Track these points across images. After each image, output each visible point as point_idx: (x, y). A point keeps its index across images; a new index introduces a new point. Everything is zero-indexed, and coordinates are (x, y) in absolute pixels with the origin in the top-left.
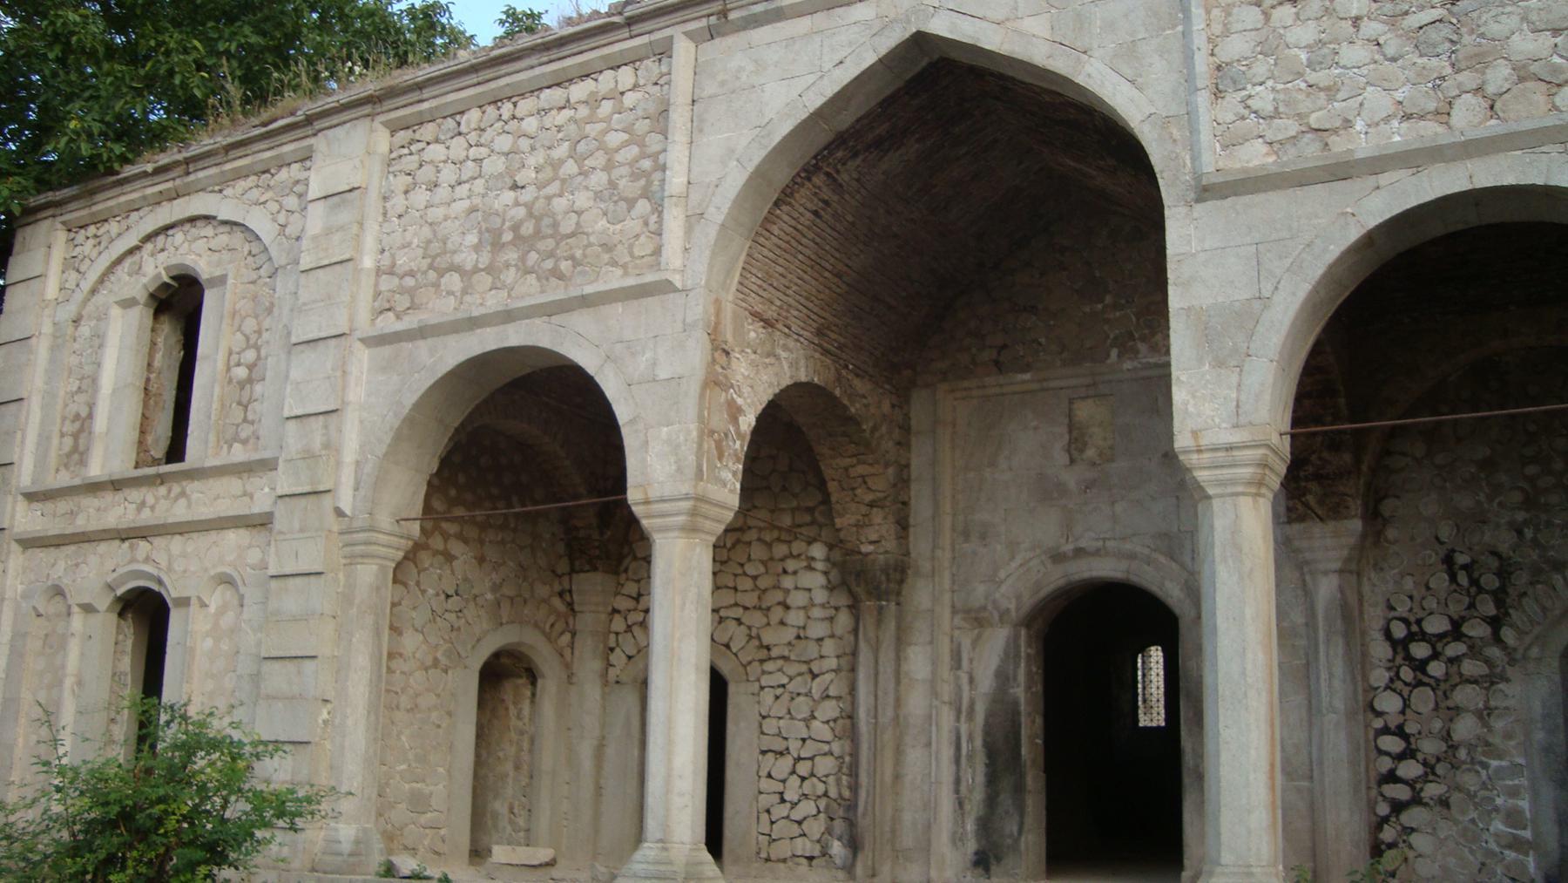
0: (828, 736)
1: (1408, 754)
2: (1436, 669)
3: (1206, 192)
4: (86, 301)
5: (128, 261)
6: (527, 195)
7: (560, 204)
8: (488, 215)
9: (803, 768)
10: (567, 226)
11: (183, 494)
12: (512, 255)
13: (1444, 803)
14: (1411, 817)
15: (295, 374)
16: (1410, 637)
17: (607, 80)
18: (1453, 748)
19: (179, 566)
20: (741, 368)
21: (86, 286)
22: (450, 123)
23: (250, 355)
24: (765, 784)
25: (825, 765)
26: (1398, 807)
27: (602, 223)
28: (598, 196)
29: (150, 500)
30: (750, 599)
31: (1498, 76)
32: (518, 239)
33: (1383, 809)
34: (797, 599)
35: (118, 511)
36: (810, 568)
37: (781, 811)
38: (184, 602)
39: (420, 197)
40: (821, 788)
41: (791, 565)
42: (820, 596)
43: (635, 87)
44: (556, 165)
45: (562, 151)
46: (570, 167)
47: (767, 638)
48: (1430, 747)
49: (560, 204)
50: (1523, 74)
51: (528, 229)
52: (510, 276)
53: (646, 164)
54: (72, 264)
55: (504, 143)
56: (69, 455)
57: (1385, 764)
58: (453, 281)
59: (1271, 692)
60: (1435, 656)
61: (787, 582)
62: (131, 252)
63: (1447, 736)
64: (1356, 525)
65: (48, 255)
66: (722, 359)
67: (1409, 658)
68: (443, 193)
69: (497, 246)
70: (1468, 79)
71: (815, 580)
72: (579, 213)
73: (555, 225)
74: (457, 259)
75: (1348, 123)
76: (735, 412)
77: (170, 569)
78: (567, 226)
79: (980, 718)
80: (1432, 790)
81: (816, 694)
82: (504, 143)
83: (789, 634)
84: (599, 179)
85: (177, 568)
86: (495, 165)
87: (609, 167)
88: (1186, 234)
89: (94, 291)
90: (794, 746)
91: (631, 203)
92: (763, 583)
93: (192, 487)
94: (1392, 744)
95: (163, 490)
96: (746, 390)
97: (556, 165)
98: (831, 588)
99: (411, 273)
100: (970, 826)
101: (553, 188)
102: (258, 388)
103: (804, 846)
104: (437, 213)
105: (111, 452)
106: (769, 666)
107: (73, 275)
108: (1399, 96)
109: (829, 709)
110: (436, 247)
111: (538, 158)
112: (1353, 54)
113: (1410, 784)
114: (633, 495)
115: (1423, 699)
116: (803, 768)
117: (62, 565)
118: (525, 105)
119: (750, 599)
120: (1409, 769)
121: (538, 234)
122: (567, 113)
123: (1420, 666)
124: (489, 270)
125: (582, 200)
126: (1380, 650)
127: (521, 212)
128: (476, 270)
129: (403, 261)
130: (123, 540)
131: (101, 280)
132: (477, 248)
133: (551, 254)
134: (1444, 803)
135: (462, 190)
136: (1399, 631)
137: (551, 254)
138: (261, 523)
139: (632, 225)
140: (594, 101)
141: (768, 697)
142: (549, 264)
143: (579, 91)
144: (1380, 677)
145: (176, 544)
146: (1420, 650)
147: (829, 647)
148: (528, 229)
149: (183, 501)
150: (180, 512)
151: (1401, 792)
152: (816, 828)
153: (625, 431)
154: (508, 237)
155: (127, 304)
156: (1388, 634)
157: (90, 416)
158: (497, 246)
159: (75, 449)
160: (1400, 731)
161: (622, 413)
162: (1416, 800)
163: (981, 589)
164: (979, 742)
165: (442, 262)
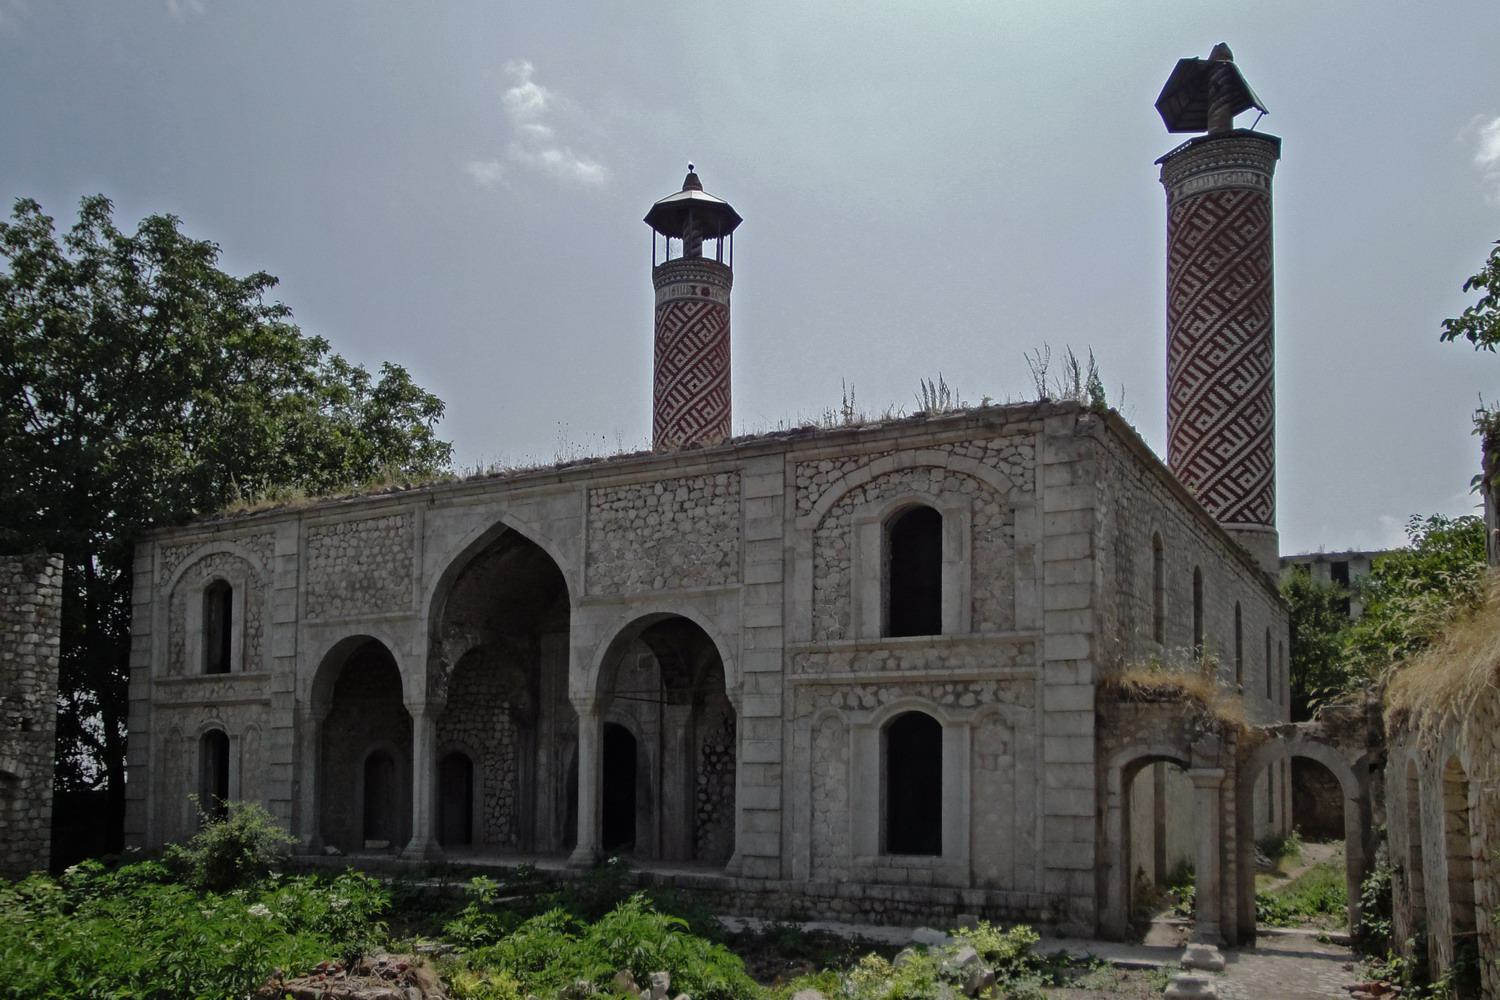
0: (509, 788)
1: (708, 801)
2: (719, 767)
3: (582, 604)
4: (175, 587)
5: (194, 568)
6: (364, 568)
7: (376, 574)
8: (350, 574)
9: (501, 802)
10: (379, 585)
11: (230, 687)
12: (359, 594)
13: (718, 821)
14: (709, 826)
15: (276, 637)
16: (711, 754)
17: (391, 522)
18: (723, 799)
19: (232, 720)
20: (447, 647)
21: (175, 578)
22: (332, 528)
23: (256, 624)
24: (487, 809)
25: (509, 801)
26: (704, 822)
27: (392, 586)
28: (390, 573)
29: (216, 689)
30: (480, 726)
31: (668, 571)
32: (362, 587)
33: (699, 823)
34: (499, 727)
35: (202, 693)
36: (503, 713)
37: (492, 821)
38: (235, 737)
39: (322, 561)
40: (507, 811)
41: (496, 711)
42: (507, 726)
43: (402, 526)
44: (375, 556)
45: (376, 550)
46: (379, 559)
47: (487, 743)
48: (715, 798)
49: (376, 574)
50: (675, 572)
51: (365, 583)
52: (359, 604)
53: (407, 562)
54: (165, 566)
55: (354, 542)
56: (175, 663)
57: (700, 805)
58: (337, 602)
59: (597, 785)
60: (719, 761)
61: (495, 719)
62: (196, 564)
63: (720, 794)
64: (690, 707)
65: (153, 561)
66: (437, 645)
67: (710, 762)
68: (331, 560)
69: (354, 590)
70: (659, 570)
71: (505, 718)
72: (384, 579)
73: (375, 584)
74: (339, 592)
75: (625, 583)
76: (444, 666)
77: (227, 722)
78: (379, 585)
79: (565, 782)
80: (715, 816)
81: (505, 769)
82: (354, 542)
83: (495, 742)
84: (390, 566)
85: (232, 722)
86: (351, 552)
87: (394, 560)
88: (577, 618)
89: (178, 582)
90: (497, 792)
91: (402, 579)
92: (485, 719)
93: (236, 684)
94: (702, 796)
95: (221, 685)
96: (450, 656)
97: (375, 556)
98: (511, 723)
99: (320, 596)
100: (561, 828)
101: (373, 567)
102: (261, 640)
103: (501, 837)
104: (330, 570)
105: (195, 663)
106: (488, 757)
107: (167, 573)
108: (641, 573)
109: (510, 776)
110: (330, 586)
111: (367, 552)
112: (629, 555)
113: (708, 812)
114: (405, 701)
115: (714, 779)
116: (501, 802)
117: (177, 717)
118: (361, 526)
119: (480, 726)
120: (708, 807)
121: (369, 587)
122: (377, 533)
123: (714, 765)
124: (352, 599)
125: (384, 574)
126: (701, 758)
127: (362, 575)
128: (346, 599)
129: (317, 589)
130: (206, 707)
131: (182, 577)
132: (346, 588)
133: (374, 596)
134: (718, 821)
135: (339, 561)
136: (708, 750)
137: (374, 596)
138: (266, 704)
139: (402, 588)
140: (388, 529)
141: (488, 770)
142: (373, 600)
143: (382, 524)
144: (700, 769)
145: (230, 710)
146: (714, 759)
147: (510, 749)
148: (365, 583)
149: (231, 691)
150: (231, 696)
151: (704, 816)
152: (506, 829)
153: (402, 676)
154: (357, 586)
155: (197, 591)
156: (704, 752)
157: (183, 645)
158: (354, 590)
159: (177, 661)
160: (705, 792)
161: (401, 668)
162: (710, 820)
163: (565, 727)
164: (565, 791)
165: (333, 593)
